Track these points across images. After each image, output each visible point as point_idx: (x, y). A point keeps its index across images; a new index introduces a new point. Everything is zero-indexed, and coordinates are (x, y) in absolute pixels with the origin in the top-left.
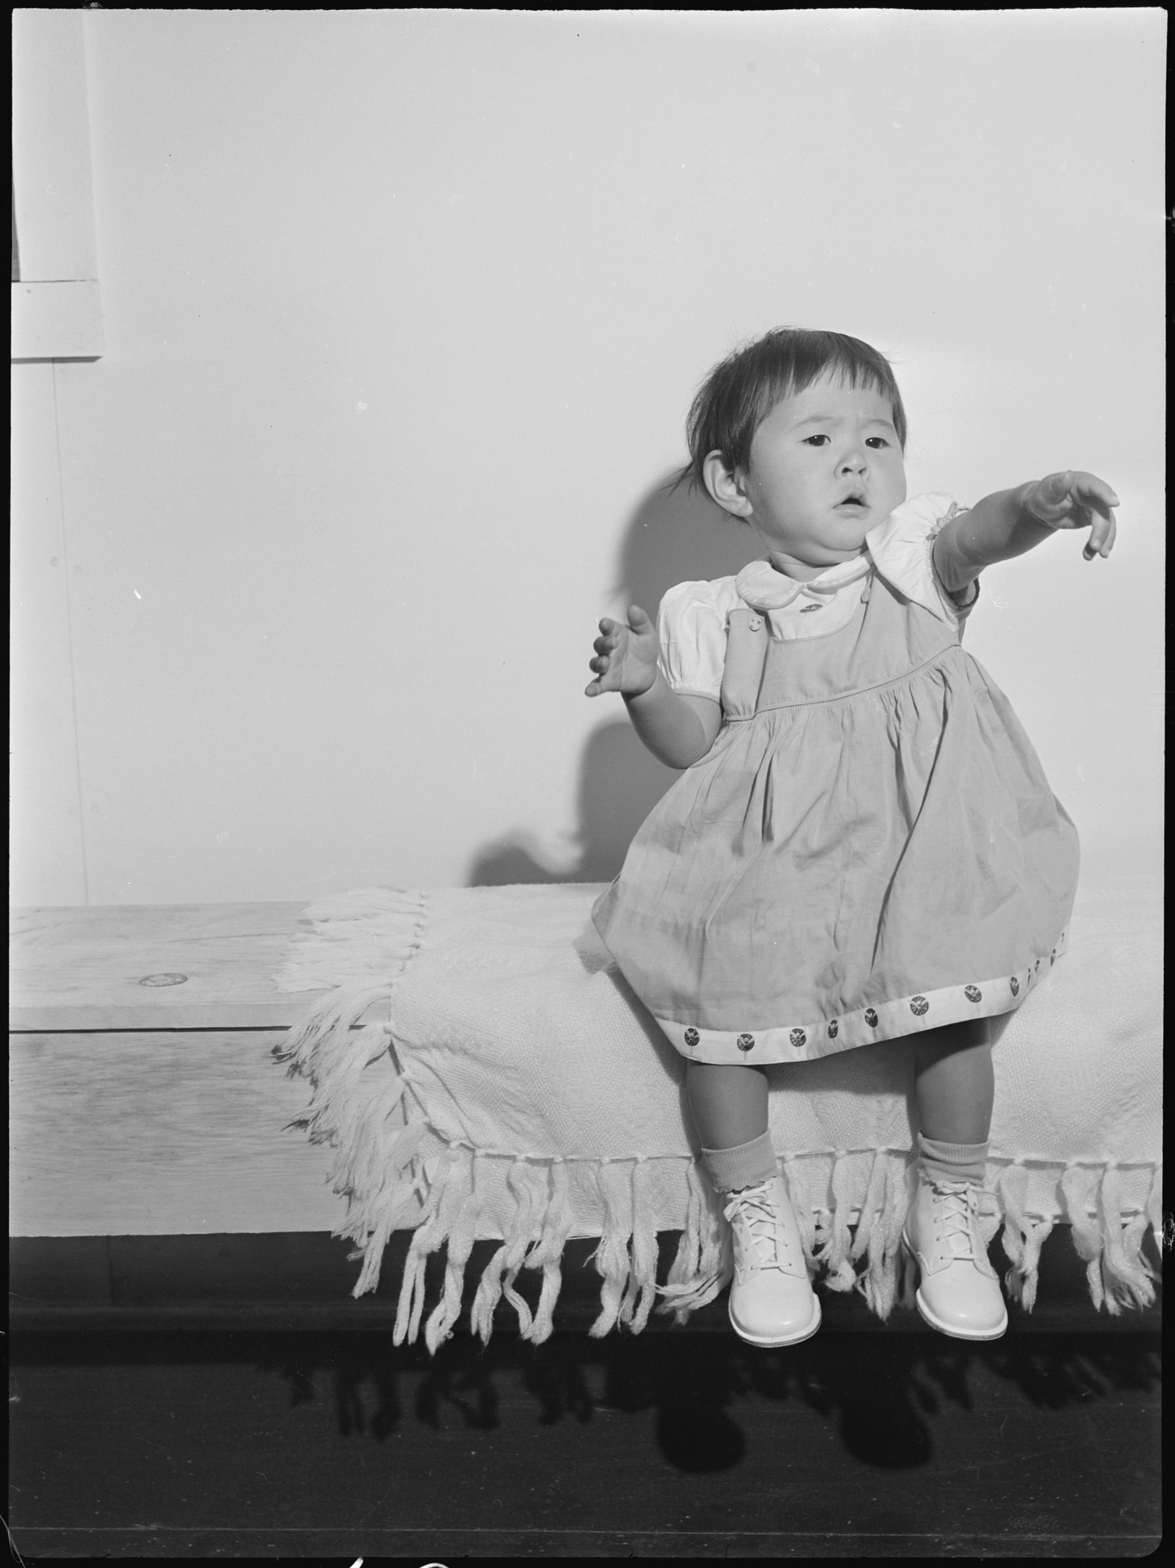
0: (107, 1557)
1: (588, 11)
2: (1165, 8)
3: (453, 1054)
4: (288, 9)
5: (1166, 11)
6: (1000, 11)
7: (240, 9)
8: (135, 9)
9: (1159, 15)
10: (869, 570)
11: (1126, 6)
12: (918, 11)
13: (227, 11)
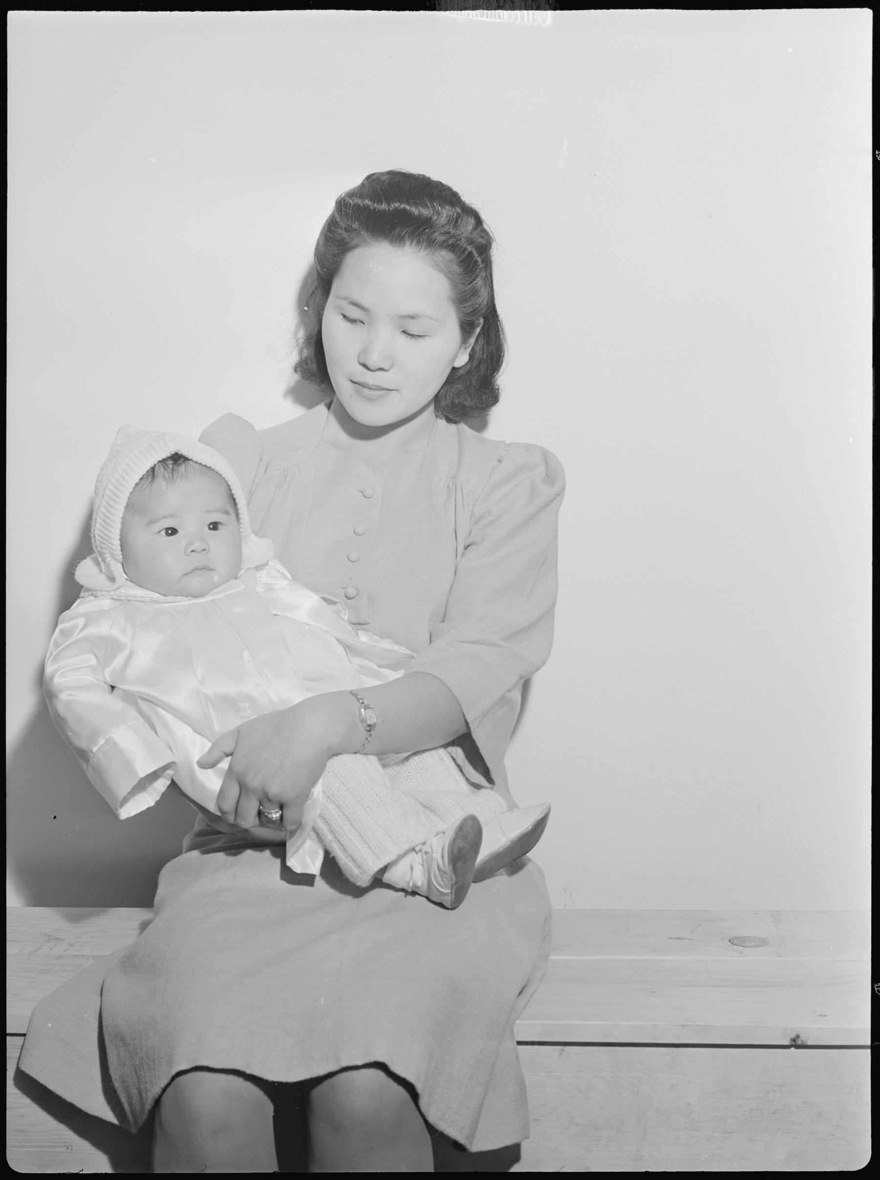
0: (81, 1173)
1: (324, 11)
2: (871, 9)
3: (529, 1137)
4: (213, 10)
5: (871, 11)
6: (747, 10)
7: (178, 11)
8: (100, 11)
9: (864, 16)
10: (466, 424)
11: (841, 8)
12: (685, 11)
13: (635, 10)
